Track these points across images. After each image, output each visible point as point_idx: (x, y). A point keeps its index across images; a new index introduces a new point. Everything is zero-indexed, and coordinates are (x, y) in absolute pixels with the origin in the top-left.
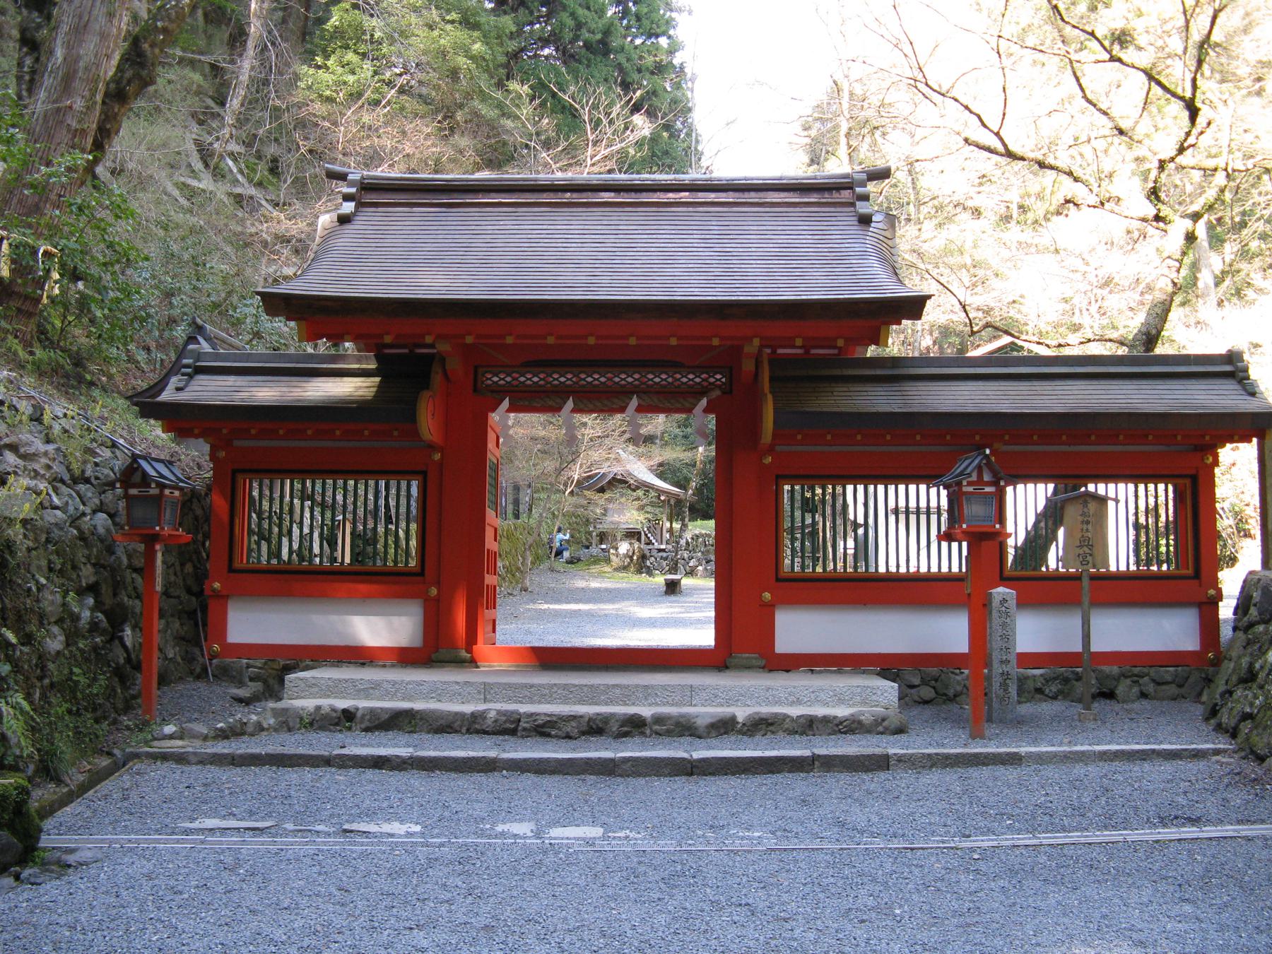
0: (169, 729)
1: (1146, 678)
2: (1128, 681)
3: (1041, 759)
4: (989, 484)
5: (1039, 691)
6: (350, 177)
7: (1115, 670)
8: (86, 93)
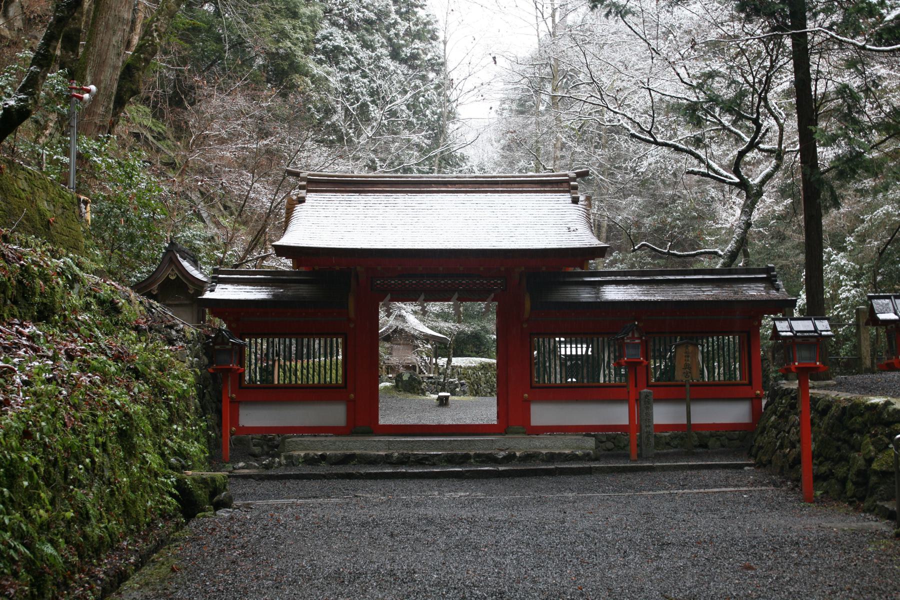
0: (241, 464)
1: (724, 437)
2: (714, 439)
3: (663, 469)
4: (637, 338)
5: (668, 444)
6: (301, 175)
7: (708, 433)
8: (106, 104)
